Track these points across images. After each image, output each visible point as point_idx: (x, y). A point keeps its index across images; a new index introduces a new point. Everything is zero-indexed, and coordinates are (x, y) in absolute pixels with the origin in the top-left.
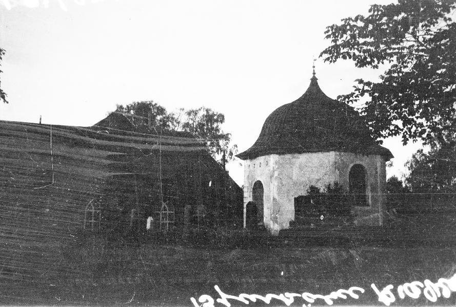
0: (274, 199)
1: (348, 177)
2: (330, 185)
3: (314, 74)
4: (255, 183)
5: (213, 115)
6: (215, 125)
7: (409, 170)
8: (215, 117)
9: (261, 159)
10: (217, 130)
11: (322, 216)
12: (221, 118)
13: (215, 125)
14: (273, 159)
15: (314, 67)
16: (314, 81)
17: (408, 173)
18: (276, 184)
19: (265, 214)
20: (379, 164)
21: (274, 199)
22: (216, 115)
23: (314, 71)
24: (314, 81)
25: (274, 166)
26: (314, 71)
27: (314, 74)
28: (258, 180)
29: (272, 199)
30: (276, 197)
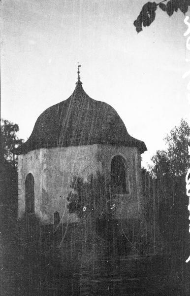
0: (43, 190)
1: (110, 166)
2: (92, 175)
3: (79, 78)
4: (113, 160)
5: (10, 125)
6: (12, 133)
7: (154, 162)
8: (12, 127)
9: (32, 154)
10: (14, 136)
11: (85, 207)
12: (16, 128)
13: (12, 133)
14: (42, 152)
15: (79, 72)
16: (79, 84)
17: (153, 165)
18: (45, 176)
19: (35, 205)
20: (136, 156)
21: (43, 190)
22: (12, 125)
23: (79, 76)
24: (79, 84)
25: (43, 159)
26: (79, 76)
27: (79, 78)
28: (29, 172)
29: (41, 190)
30: (46, 189)
